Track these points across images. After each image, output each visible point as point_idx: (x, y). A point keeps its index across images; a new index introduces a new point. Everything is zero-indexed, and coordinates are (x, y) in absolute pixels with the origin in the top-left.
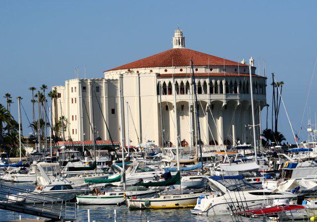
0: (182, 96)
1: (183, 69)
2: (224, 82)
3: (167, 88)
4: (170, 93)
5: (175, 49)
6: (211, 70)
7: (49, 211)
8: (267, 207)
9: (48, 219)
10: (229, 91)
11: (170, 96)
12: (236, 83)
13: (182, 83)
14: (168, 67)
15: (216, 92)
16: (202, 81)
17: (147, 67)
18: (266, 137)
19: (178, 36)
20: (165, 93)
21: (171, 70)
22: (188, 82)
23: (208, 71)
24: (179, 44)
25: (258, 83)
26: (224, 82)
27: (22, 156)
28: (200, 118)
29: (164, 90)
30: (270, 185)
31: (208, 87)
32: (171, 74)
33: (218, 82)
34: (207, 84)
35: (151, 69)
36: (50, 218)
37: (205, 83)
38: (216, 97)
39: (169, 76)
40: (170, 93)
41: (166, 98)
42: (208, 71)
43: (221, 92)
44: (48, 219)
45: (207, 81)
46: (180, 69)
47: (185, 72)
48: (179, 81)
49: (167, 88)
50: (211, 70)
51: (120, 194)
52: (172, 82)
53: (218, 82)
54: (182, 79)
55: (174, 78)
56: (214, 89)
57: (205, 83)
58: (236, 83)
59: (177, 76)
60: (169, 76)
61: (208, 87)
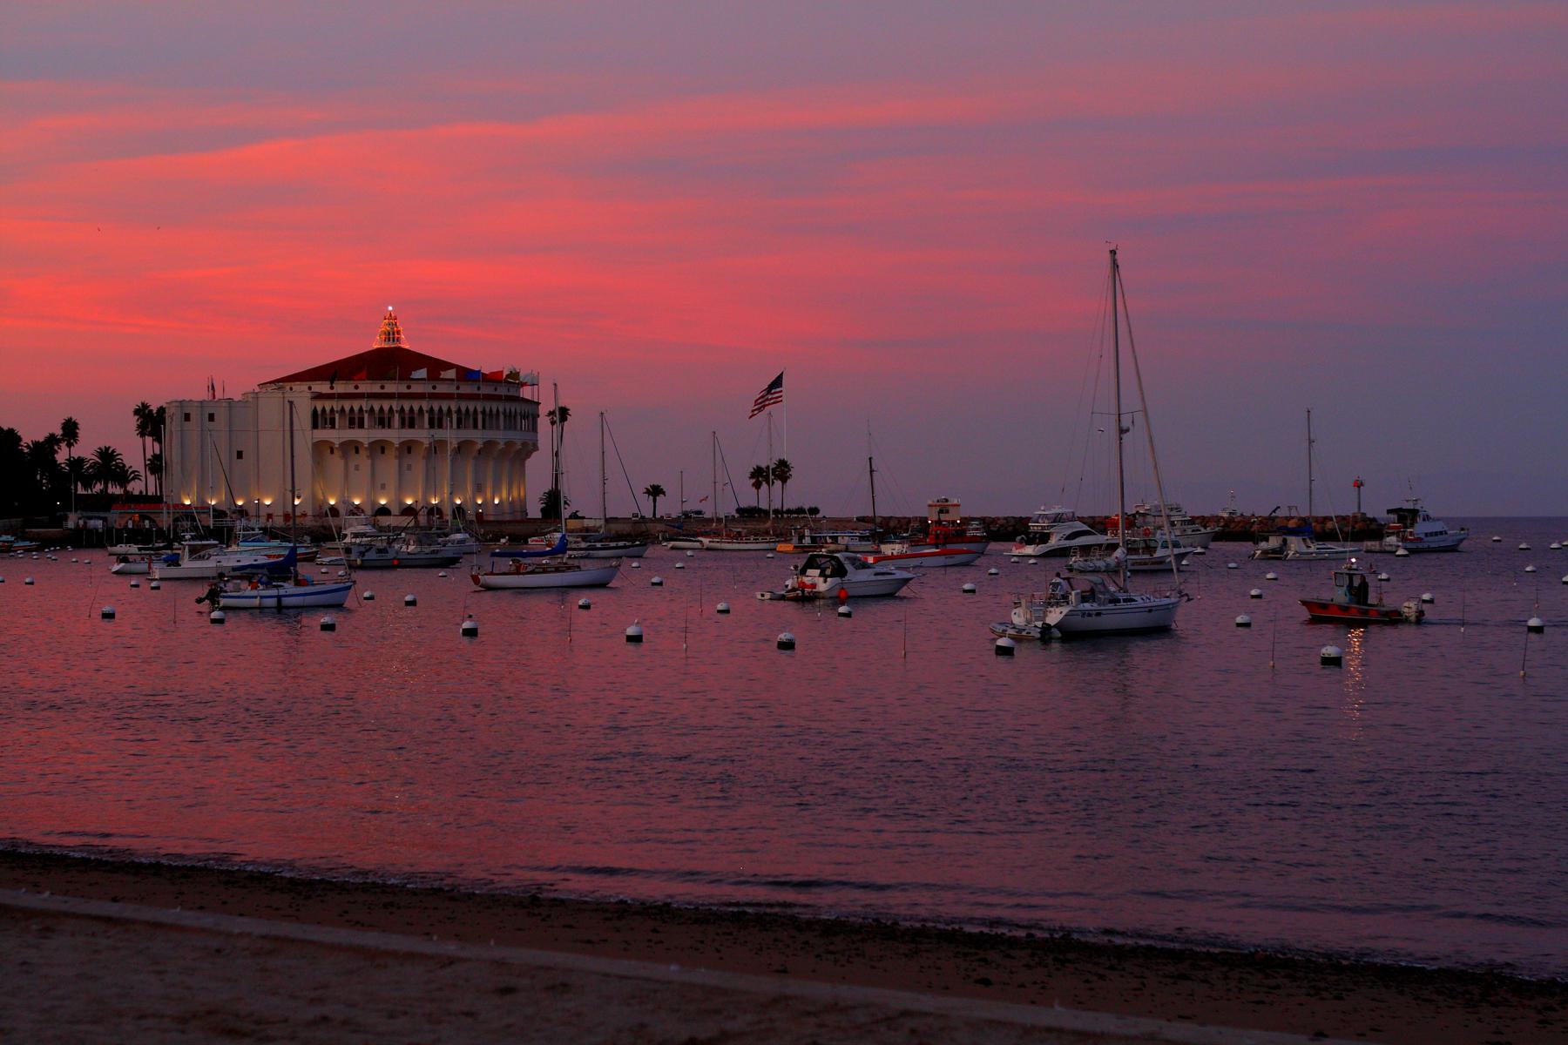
0: (412, 430)
3: (436, 417)
7: (334, 558)
10: (320, 425)
12: (498, 411)
14: (314, 383)
17: (377, 379)
21: (366, 387)
25: (530, 412)
29: (318, 420)
30: (822, 586)
32: (394, 394)
34: (479, 413)
40: (333, 427)
41: (323, 434)
48: (347, 405)
49: (436, 417)
51: (1193, 531)
56: (436, 421)
58: (498, 411)
59: (402, 396)
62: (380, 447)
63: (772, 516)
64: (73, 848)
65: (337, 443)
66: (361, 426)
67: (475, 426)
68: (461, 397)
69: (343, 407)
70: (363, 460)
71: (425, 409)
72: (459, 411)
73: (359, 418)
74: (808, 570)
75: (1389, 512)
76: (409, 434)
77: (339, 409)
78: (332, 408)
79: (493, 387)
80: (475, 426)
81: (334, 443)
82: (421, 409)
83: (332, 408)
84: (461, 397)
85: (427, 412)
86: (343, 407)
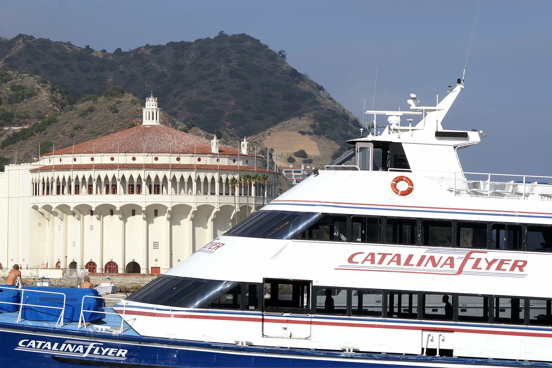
0: (157, 196)
1: (201, 158)
4: (139, 192)
6: (234, 161)
9: (452, 304)
11: (139, 195)
13: (182, 178)
14: (159, 154)
15: (227, 194)
19: (151, 107)
20: (132, 192)
22: (190, 177)
24: (153, 119)
27: (93, 265)
28: (196, 228)
31: (217, 185)
34: (193, 181)
35: (92, 155)
36: (453, 304)
37: (213, 179)
38: (228, 200)
39: (138, 167)
44: (452, 304)
45: (216, 176)
46: (154, 157)
47: (79, 163)
50: (234, 161)
54: (173, 173)
55: (196, 172)
57: (213, 179)
59: (174, 167)
60: (138, 167)
61: (217, 185)
62: (133, 210)
63: (84, 267)
64: (112, 360)
65: (118, 207)
66: (114, 192)
67: (213, 194)
68: (200, 168)
69: (123, 176)
70: (139, 219)
71: (168, 177)
72: (198, 180)
73: (113, 186)
74: (250, 307)
75: (535, 317)
76: (155, 199)
77: (120, 177)
78: (114, 177)
79: (59, 159)
80: (213, 194)
81: (115, 207)
82: (165, 178)
83: (114, 177)
84: (200, 168)
85: (145, 180)
86: (123, 176)
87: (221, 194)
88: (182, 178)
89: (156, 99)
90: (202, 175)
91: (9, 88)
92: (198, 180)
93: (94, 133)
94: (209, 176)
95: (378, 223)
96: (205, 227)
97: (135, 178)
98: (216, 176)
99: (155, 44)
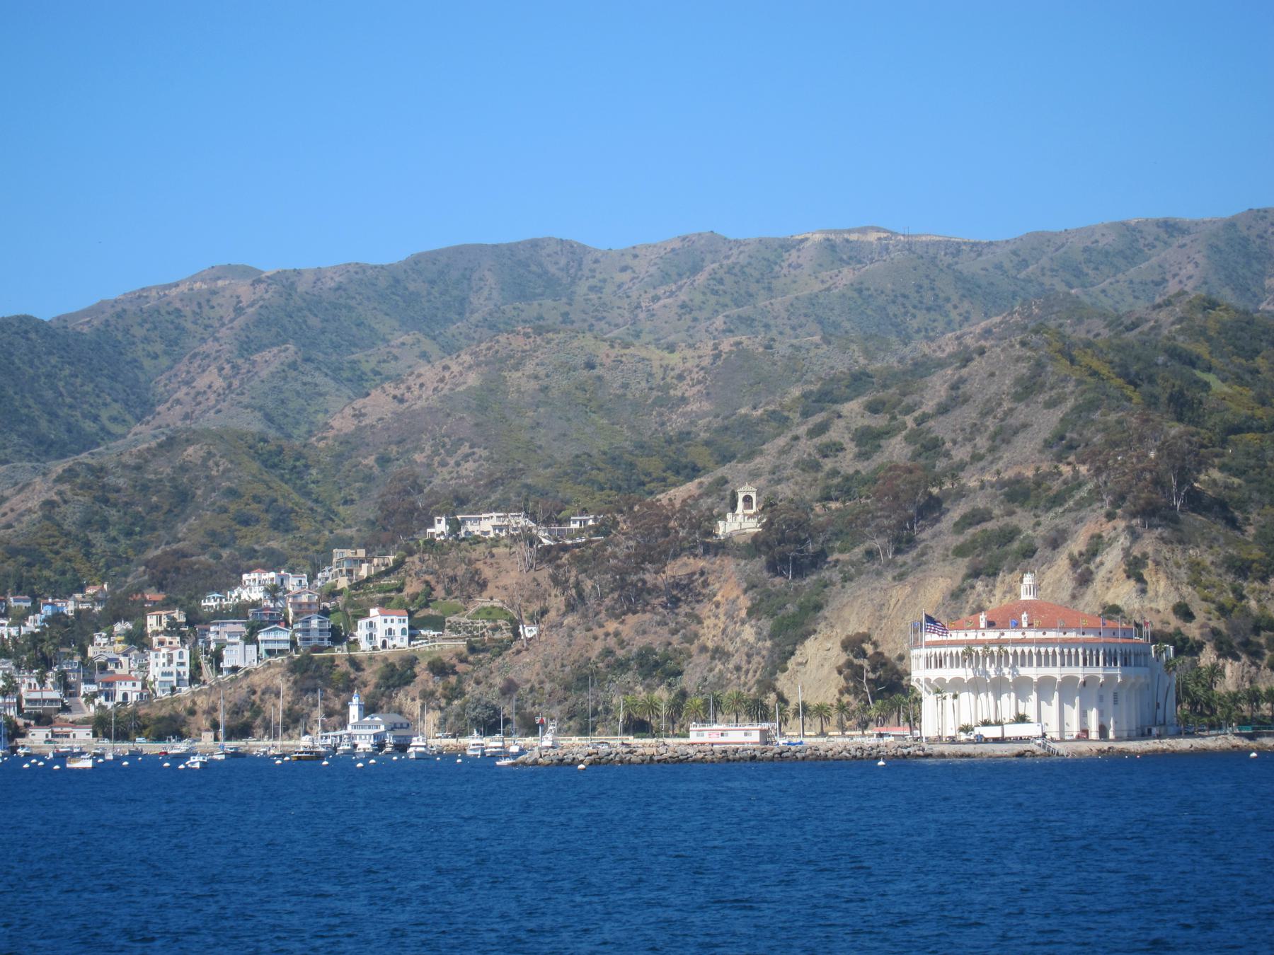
2: (1080, 650)
5: (1026, 601)
8: (215, 757)
13: (1023, 652)
15: (1070, 664)
16: (1050, 650)
18: (267, 759)
23: (1061, 635)
26: (1080, 650)
31: (1058, 658)
33: (1073, 651)
38: (1091, 671)
39: (1029, 642)
42: (1061, 635)
43: (1098, 664)
52: (1033, 650)
53: (1073, 651)
57: (1054, 652)
59: (1040, 643)
61: (1058, 658)
72: (1039, 653)
87: (1063, 665)
88: (1023, 652)
89: (904, 682)
90: (1019, 650)
91: (259, 415)
92: (1039, 653)
93: (1084, 791)
94: (1026, 649)
95: (333, 656)
96: (1049, 704)
97: (954, 653)
98: (1033, 649)
99: (972, 240)
